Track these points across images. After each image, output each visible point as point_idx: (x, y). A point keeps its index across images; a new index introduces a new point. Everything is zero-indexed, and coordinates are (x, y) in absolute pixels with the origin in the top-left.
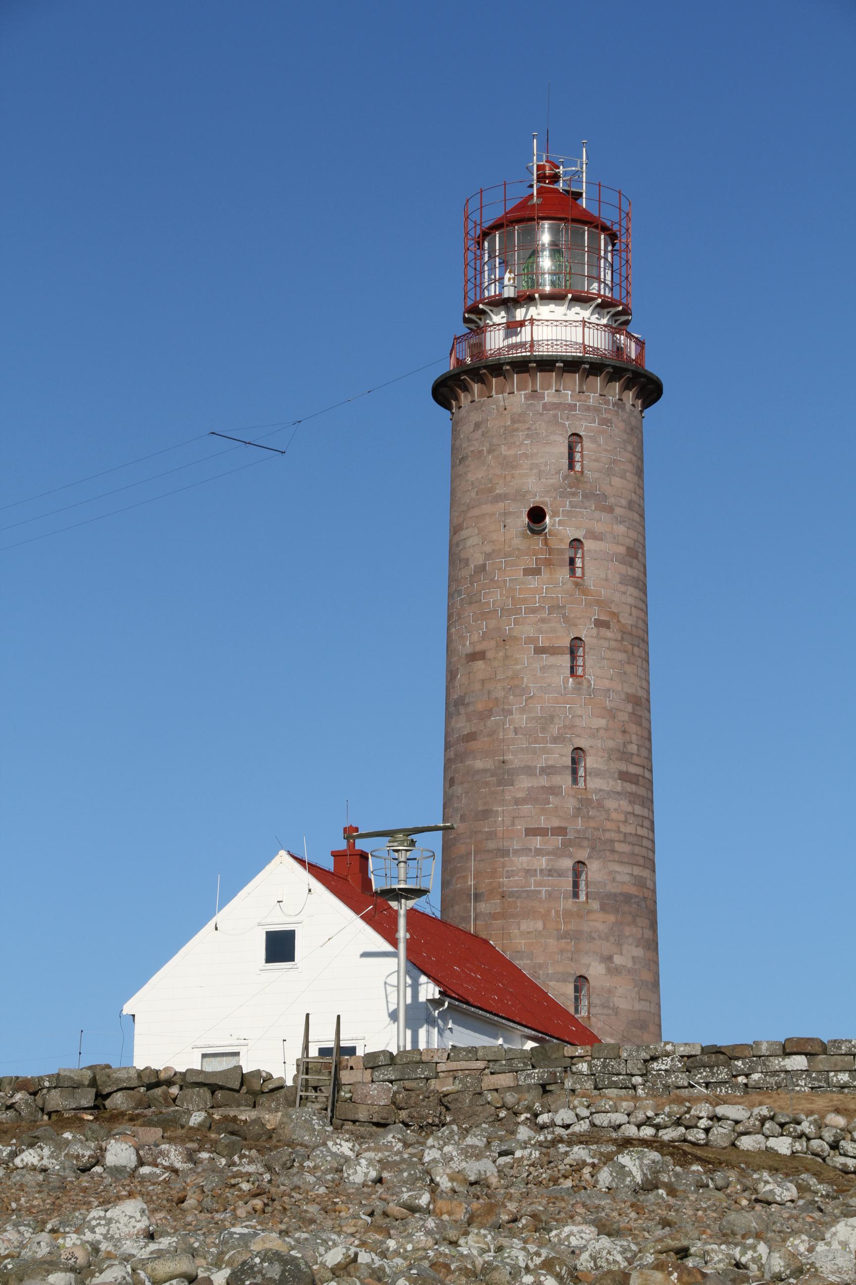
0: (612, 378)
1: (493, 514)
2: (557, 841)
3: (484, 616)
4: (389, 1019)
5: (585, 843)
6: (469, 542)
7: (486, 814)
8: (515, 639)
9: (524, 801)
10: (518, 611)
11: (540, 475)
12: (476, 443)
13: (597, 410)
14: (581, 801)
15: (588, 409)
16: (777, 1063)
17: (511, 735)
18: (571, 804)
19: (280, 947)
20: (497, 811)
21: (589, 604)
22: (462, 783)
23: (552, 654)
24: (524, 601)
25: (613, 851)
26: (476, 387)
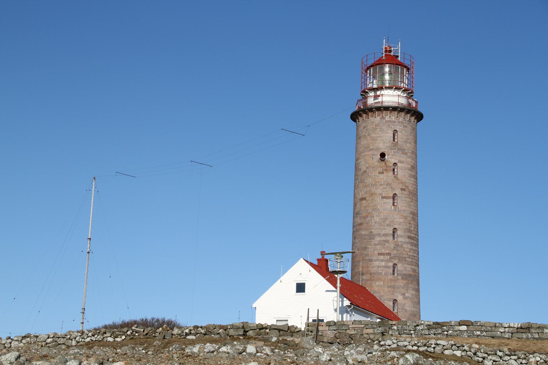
3: (366, 186)
5: (397, 258)
6: (361, 164)
7: (365, 248)
8: (375, 194)
10: (376, 185)
11: (384, 143)
13: (402, 123)
14: (395, 245)
15: (399, 122)
16: (457, 328)
17: (374, 224)
18: (392, 246)
19: (301, 288)
21: (399, 183)
24: (378, 182)
25: (406, 261)
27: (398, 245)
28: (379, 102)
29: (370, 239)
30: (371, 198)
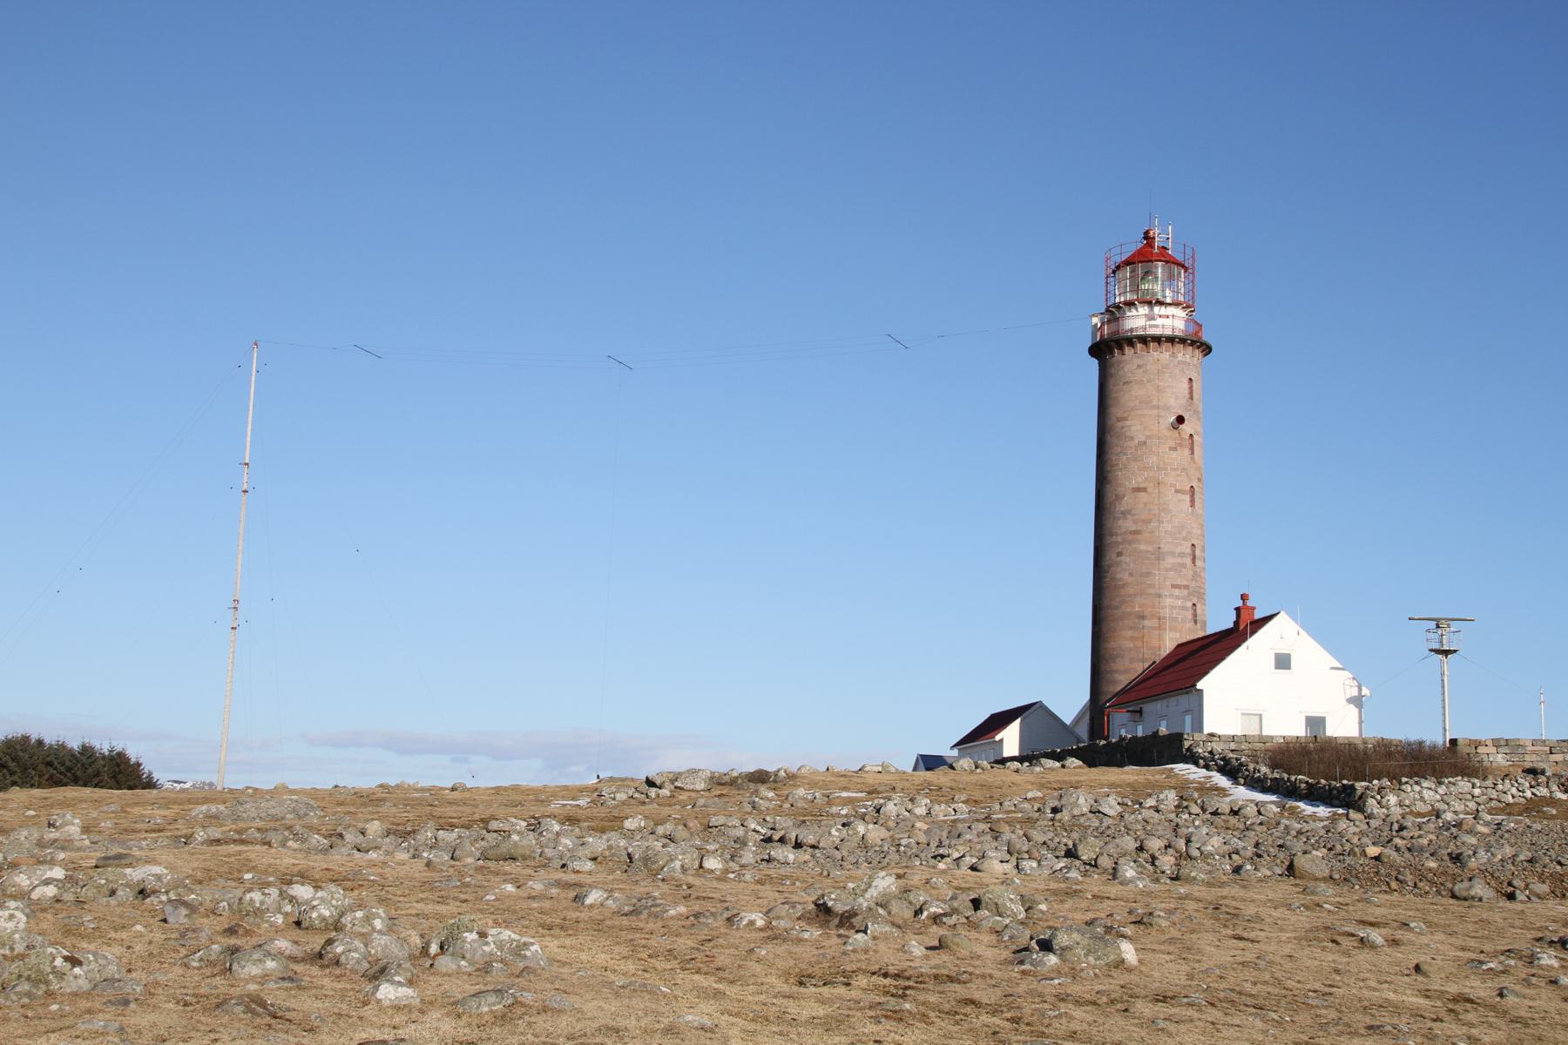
3: (1145, 469)
7: (1148, 574)
19: (1283, 662)
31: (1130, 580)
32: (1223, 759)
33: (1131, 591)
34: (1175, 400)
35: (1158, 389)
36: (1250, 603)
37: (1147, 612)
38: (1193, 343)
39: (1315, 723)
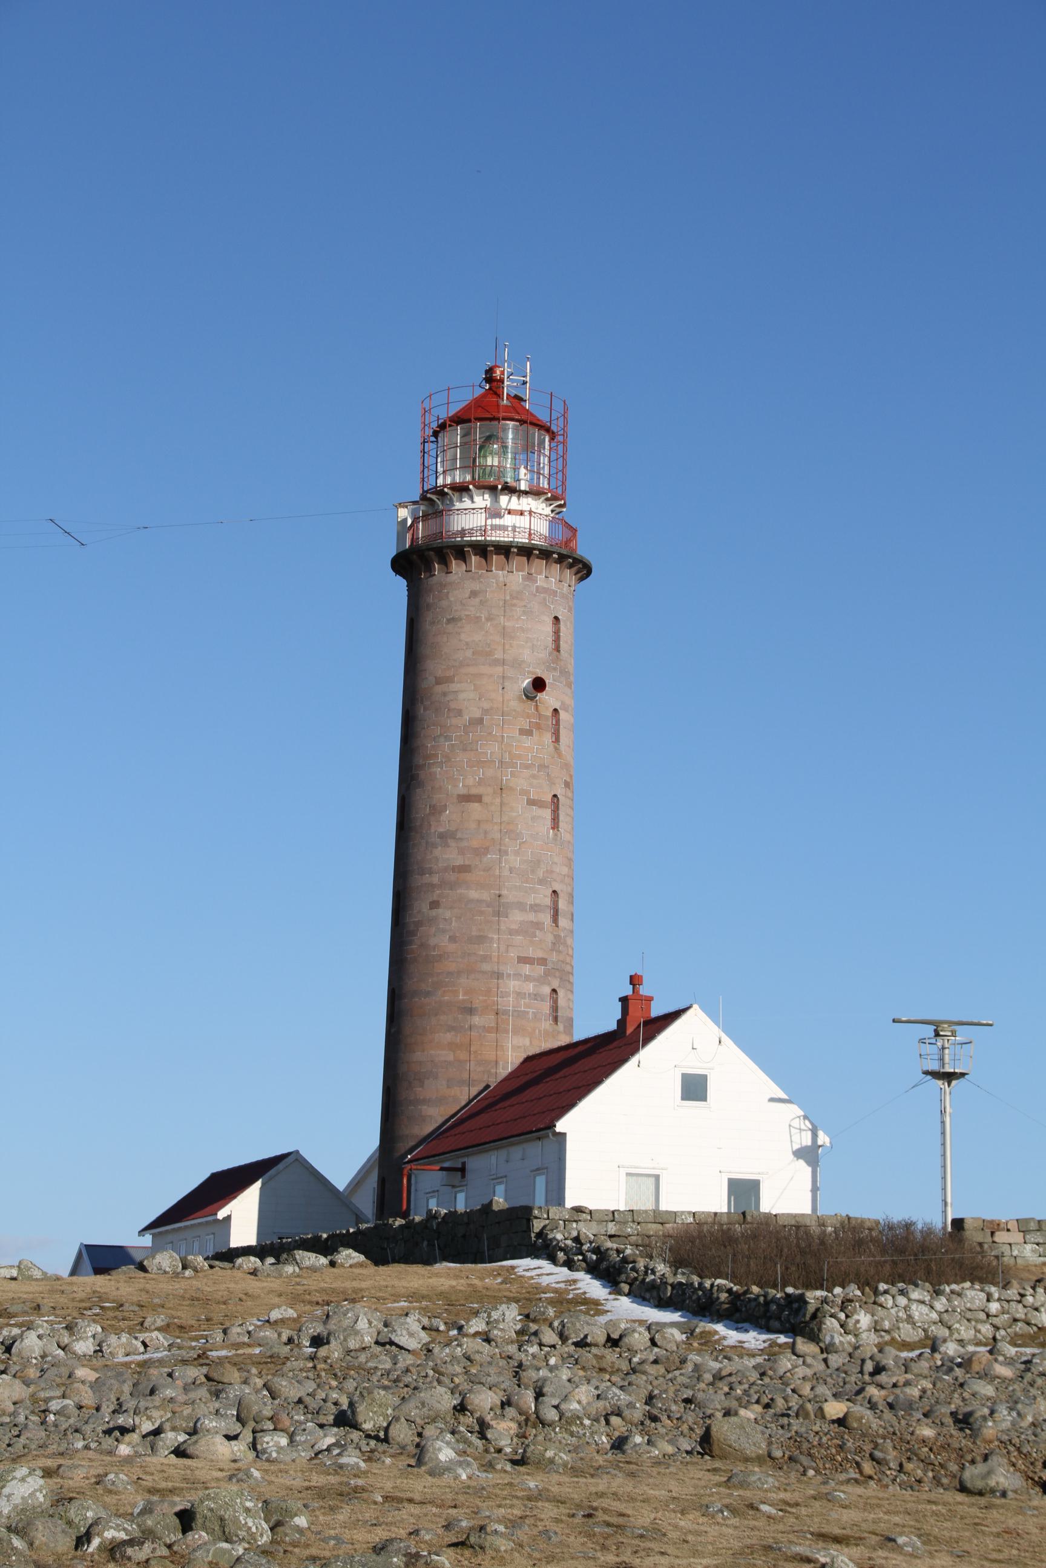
0: (571, 566)
1: (491, 676)
2: (540, 970)
3: (480, 764)
4: (792, 1156)
5: (557, 974)
6: (462, 696)
7: (481, 939)
8: (511, 789)
9: (517, 932)
10: (514, 765)
12: (472, 609)
15: (563, 596)
17: (506, 873)
18: (550, 938)
19: (694, 1088)
20: (492, 938)
22: (451, 908)
23: (540, 807)
24: (519, 757)
26: (474, 559)
27: (559, 936)
28: (504, 528)
29: (498, 914)
30: (498, 800)
31: (451, 947)
32: (597, 1250)
33: (452, 967)
34: (532, 656)
35: (504, 633)
36: (644, 990)
37: (478, 1001)
38: (562, 559)
39: (744, 1190)
